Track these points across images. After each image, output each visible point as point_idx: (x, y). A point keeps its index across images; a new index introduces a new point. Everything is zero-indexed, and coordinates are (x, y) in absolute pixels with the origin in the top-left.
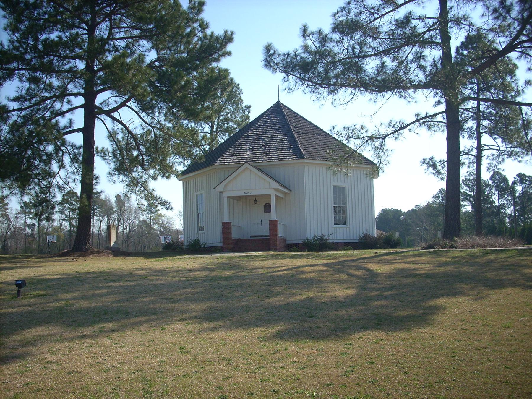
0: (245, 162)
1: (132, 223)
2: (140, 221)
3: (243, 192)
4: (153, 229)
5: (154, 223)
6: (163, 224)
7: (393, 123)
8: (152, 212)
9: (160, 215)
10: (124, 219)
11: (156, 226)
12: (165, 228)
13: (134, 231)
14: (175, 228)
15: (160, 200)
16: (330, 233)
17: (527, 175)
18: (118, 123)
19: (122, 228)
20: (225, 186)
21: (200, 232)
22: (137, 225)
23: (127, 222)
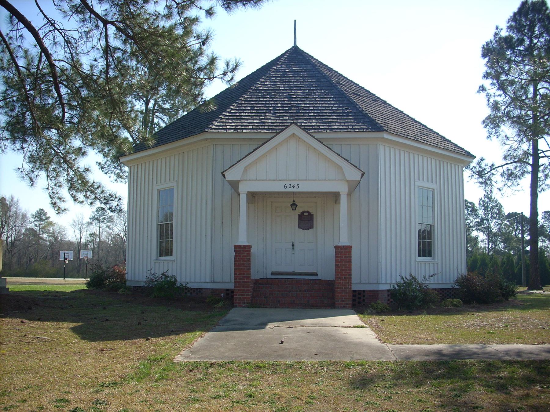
0: (292, 123)
1: (17, 231)
2: (26, 230)
3: (283, 183)
4: (42, 238)
5: (44, 232)
6: (53, 233)
7: (57, 212)
8: (41, 220)
9: (51, 224)
10: (8, 226)
11: (45, 236)
12: (56, 239)
13: (19, 240)
14: (67, 239)
15: (99, 191)
16: (432, 273)
17: (469, 201)
18: (21, 25)
19: (6, 236)
20: (246, 169)
21: (163, 258)
22: (24, 234)
23: (12, 229)
